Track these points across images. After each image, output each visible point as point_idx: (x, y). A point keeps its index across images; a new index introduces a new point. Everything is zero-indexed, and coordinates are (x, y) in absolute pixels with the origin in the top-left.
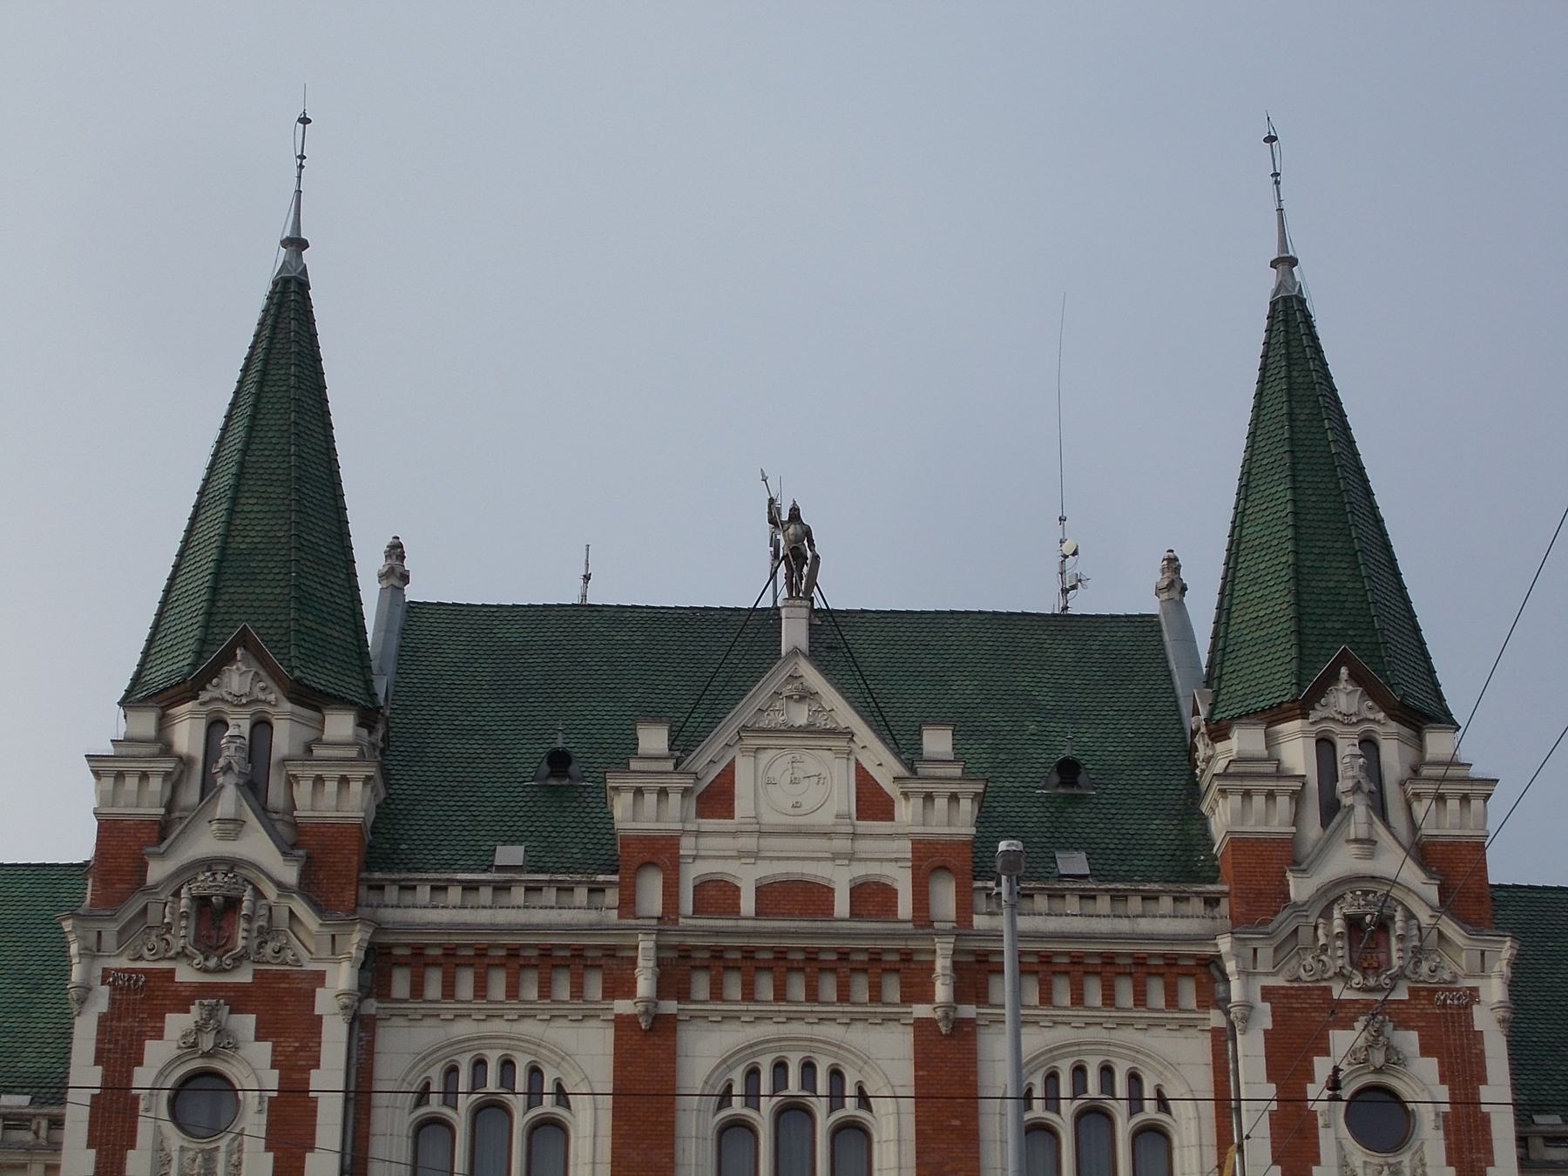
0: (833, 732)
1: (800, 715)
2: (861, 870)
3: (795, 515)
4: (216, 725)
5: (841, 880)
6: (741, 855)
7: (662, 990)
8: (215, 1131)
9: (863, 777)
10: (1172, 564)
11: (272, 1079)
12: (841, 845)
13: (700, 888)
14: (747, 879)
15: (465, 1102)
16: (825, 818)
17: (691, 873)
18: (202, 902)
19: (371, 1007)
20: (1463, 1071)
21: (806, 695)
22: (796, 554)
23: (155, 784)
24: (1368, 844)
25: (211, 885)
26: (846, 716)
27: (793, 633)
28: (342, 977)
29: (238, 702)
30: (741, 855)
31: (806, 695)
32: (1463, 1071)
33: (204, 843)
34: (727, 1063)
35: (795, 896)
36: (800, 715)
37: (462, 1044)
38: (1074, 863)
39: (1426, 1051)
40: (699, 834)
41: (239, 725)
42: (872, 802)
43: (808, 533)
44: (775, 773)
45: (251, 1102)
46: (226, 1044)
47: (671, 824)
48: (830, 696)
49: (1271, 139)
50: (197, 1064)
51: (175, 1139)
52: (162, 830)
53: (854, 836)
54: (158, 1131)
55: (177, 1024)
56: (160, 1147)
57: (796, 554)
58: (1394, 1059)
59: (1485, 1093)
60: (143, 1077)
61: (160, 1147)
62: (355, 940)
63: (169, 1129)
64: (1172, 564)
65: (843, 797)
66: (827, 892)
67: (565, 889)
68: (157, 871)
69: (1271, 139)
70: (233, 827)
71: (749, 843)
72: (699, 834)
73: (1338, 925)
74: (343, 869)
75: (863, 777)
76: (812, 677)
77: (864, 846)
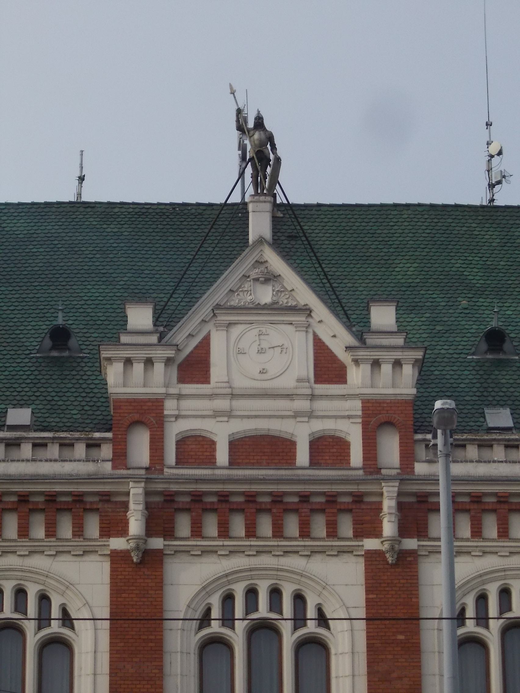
0: (294, 309)
1: (265, 295)
3: (259, 123)
5: (302, 435)
6: (216, 414)
7: (404, 531)
12: (303, 405)
14: (222, 433)
16: (287, 382)
21: (270, 278)
26: (305, 295)
27: (259, 224)
30: (216, 414)
31: (270, 278)
34: (206, 590)
40: (180, 397)
42: (328, 369)
43: (270, 138)
44: (244, 344)
48: (291, 279)
53: (313, 397)
57: (261, 157)
64: (230, 85)
65: (303, 364)
71: (222, 404)
72: (180, 397)
76: (276, 263)
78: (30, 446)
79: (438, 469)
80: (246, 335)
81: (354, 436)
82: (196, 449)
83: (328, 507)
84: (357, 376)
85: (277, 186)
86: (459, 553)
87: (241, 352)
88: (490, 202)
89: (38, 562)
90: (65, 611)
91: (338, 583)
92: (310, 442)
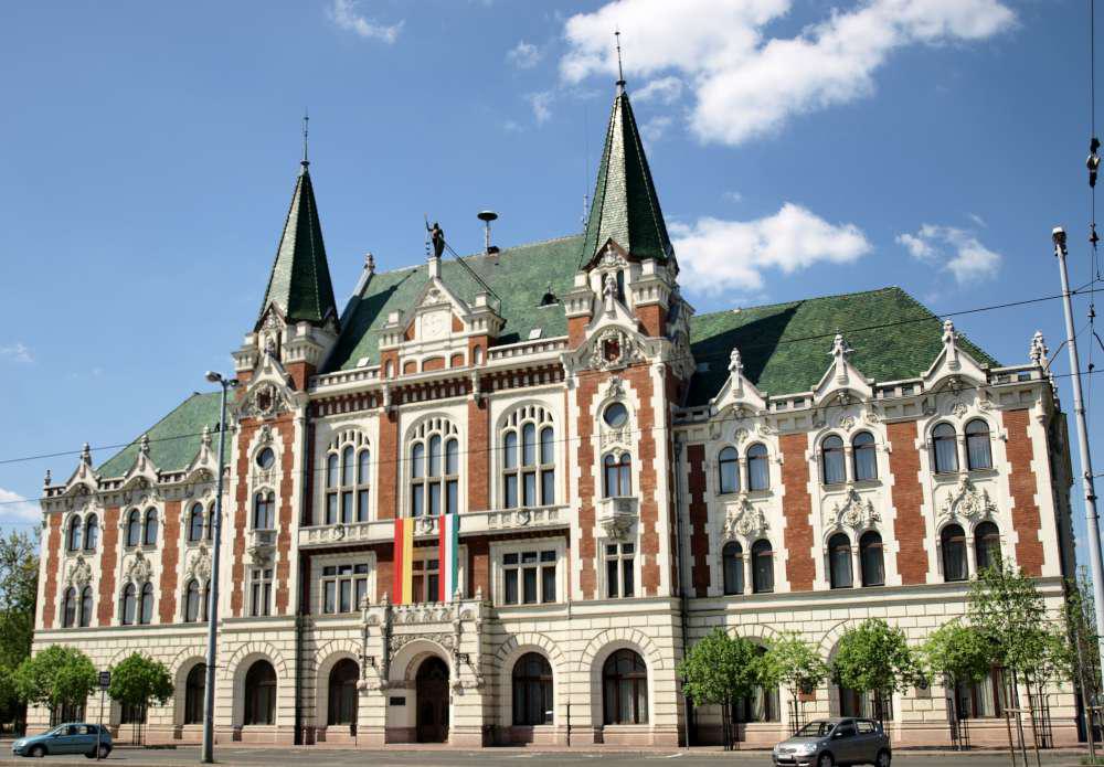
0: (446, 304)
1: (433, 300)
2: (453, 351)
3: (436, 226)
4: (604, 276)
5: (447, 355)
7: (482, 390)
14: (419, 359)
18: (605, 343)
20: (645, 393)
21: (436, 293)
24: (269, 370)
26: (449, 298)
28: (299, 413)
29: (611, 265)
31: (436, 293)
32: (645, 393)
36: (433, 300)
38: (736, 311)
39: (632, 387)
40: (404, 348)
41: (613, 275)
42: (457, 326)
43: (440, 232)
44: (427, 321)
47: (396, 345)
50: (613, 401)
51: (607, 429)
54: (601, 427)
55: (258, 433)
58: (620, 392)
63: (256, 465)
66: (443, 358)
71: (418, 348)
77: (455, 343)
78: (775, 405)
79: (838, 347)
81: (466, 351)
82: (410, 365)
86: (972, 435)
87: (427, 324)
88: (338, 333)
90: (367, 438)
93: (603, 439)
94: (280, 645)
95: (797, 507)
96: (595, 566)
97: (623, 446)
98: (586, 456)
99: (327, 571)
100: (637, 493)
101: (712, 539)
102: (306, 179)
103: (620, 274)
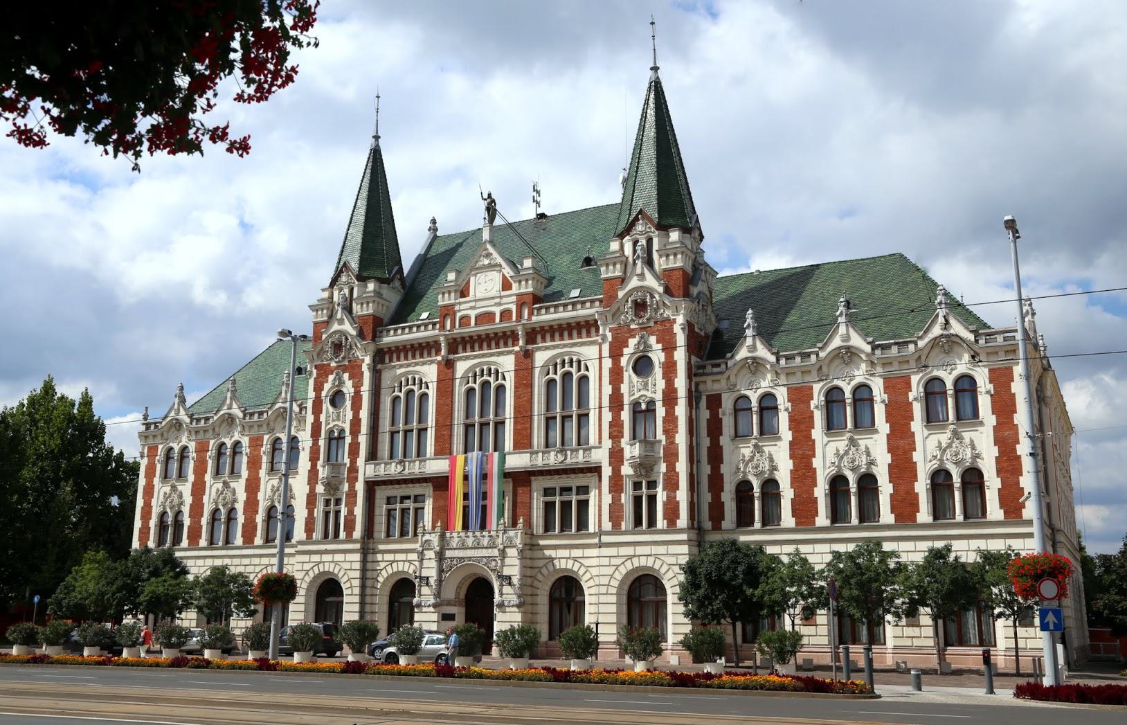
1: (486, 262)
3: (490, 196)
4: (635, 243)
5: (497, 310)
6: (496, 304)
8: (648, 376)
9: (504, 277)
10: (434, 221)
11: (352, 390)
12: (497, 300)
13: (461, 319)
14: (473, 314)
15: (559, 373)
16: (493, 293)
17: (458, 315)
19: (379, 366)
20: (669, 348)
22: (491, 211)
23: (618, 266)
25: (637, 296)
26: (499, 260)
27: (486, 235)
28: (368, 360)
29: (642, 233)
30: (496, 304)
32: (669, 348)
33: (634, 283)
34: (467, 371)
35: (486, 317)
37: (409, 373)
40: (460, 303)
41: (643, 242)
42: (506, 285)
43: (493, 201)
45: (347, 396)
46: (341, 383)
48: (495, 255)
49: (652, 23)
51: (635, 378)
52: (327, 323)
53: (501, 297)
56: (630, 382)
57: (491, 211)
58: (648, 347)
59: (362, 389)
60: (324, 394)
61: (630, 382)
62: (372, 347)
64: (434, 221)
65: (499, 285)
67: (547, 308)
68: (621, 294)
69: (652, 23)
70: (341, 322)
71: (472, 304)
72: (460, 303)
73: (629, 304)
74: (373, 328)
75: (504, 277)
76: (490, 249)
77: (504, 300)
80: (481, 277)
81: (513, 308)
82: (465, 320)
83: (503, 338)
84: (515, 286)
85: (432, 253)
89: (417, 368)
91: (507, 363)
92: (935, 284)
93: (632, 387)
94: (347, 566)
95: (802, 451)
96: (623, 501)
97: (649, 394)
98: (616, 402)
99: (548, 492)
100: (661, 436)
101: (727, 479)
102: (657, 89)
103: (650, 241)
